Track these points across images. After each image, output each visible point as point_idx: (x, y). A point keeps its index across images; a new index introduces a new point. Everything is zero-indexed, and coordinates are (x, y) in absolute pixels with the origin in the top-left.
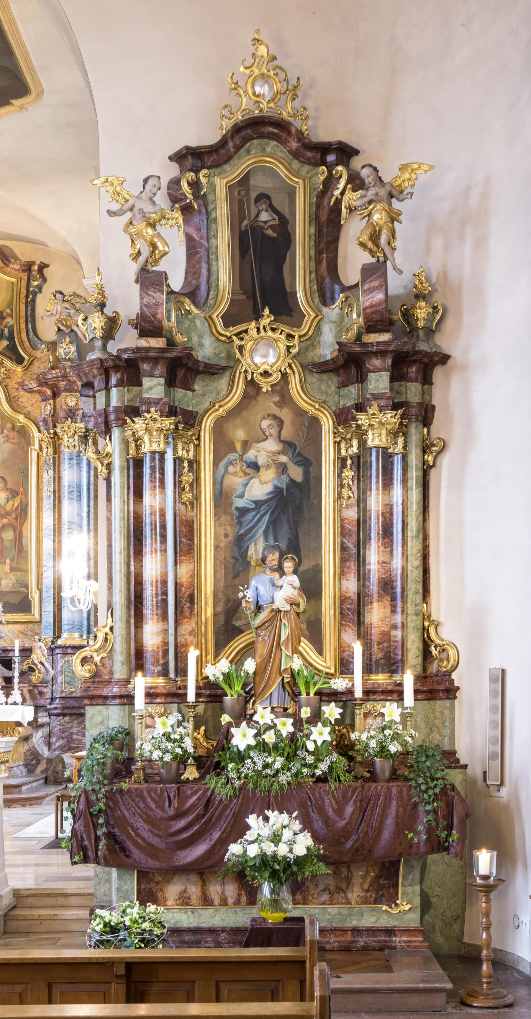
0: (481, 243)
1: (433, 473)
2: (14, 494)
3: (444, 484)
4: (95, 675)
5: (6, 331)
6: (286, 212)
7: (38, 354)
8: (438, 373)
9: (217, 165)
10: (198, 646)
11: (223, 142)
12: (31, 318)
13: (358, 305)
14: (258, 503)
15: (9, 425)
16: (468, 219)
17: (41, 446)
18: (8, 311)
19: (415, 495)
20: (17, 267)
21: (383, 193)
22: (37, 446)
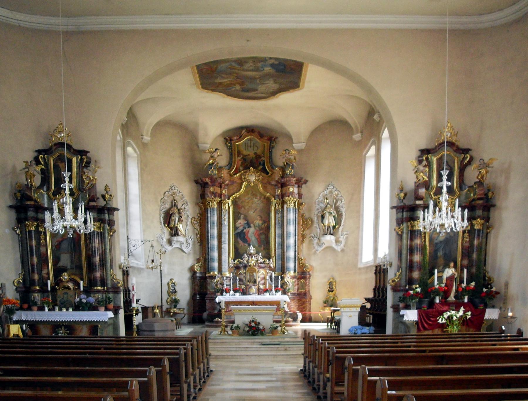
0: (507, 178)
1: (489, 235)
2: (264, 222)
3: (492, 238)
4: (396, 284)
5: (262, 162)
6: (452, 166)
7: (275, 171)
8: (492, 209)
9: (433, 153)
10: (82, 279)
11: (436, 147)
12: (271, 157)
13: (236, 69)
14: (441, 242)
15: (263, 197)
16: (507, 172)
17: (275, 205)
18: (263, 155)
19: (484, 240)
20: (266, 138)
21: (485, 166)
22: (274, 205)
